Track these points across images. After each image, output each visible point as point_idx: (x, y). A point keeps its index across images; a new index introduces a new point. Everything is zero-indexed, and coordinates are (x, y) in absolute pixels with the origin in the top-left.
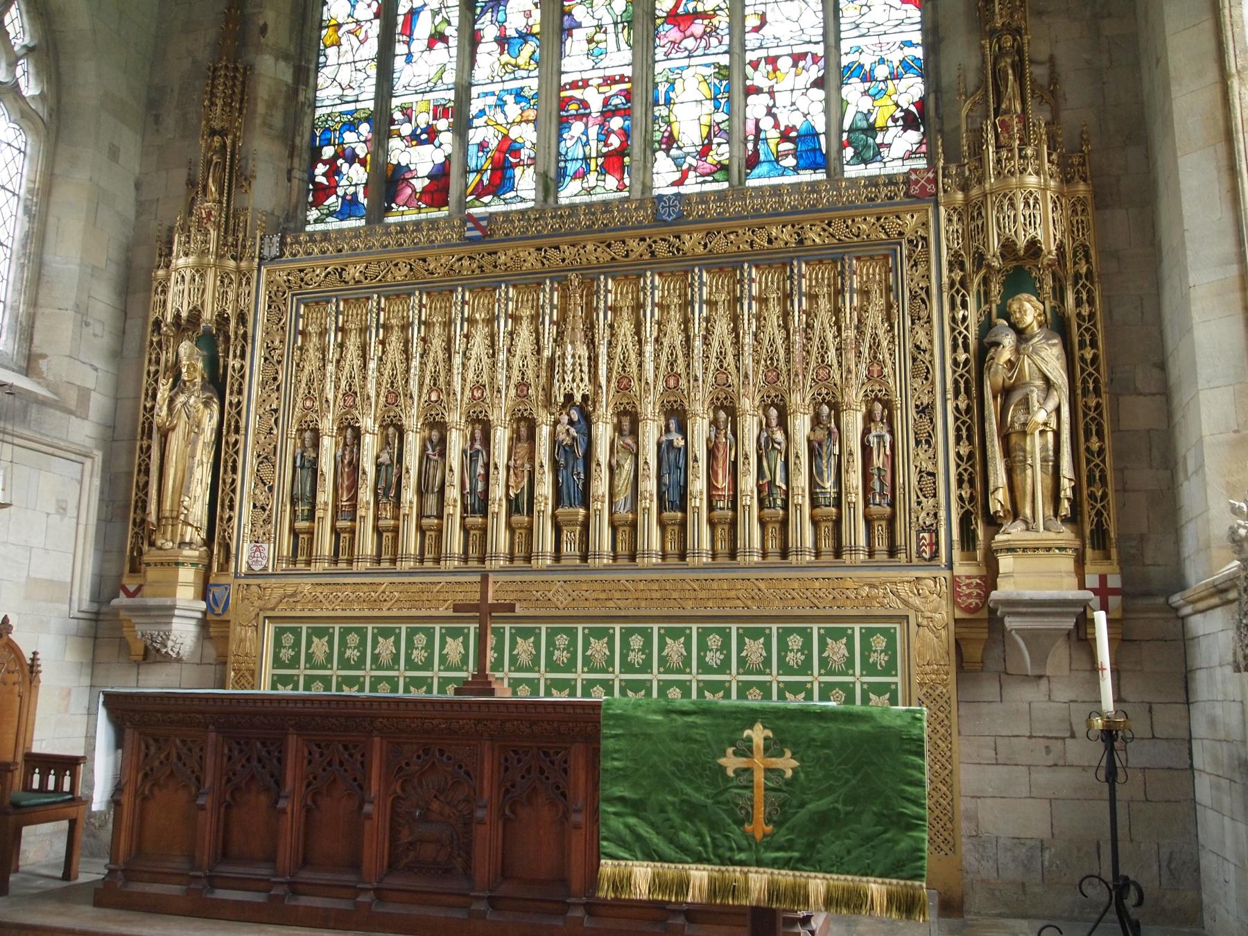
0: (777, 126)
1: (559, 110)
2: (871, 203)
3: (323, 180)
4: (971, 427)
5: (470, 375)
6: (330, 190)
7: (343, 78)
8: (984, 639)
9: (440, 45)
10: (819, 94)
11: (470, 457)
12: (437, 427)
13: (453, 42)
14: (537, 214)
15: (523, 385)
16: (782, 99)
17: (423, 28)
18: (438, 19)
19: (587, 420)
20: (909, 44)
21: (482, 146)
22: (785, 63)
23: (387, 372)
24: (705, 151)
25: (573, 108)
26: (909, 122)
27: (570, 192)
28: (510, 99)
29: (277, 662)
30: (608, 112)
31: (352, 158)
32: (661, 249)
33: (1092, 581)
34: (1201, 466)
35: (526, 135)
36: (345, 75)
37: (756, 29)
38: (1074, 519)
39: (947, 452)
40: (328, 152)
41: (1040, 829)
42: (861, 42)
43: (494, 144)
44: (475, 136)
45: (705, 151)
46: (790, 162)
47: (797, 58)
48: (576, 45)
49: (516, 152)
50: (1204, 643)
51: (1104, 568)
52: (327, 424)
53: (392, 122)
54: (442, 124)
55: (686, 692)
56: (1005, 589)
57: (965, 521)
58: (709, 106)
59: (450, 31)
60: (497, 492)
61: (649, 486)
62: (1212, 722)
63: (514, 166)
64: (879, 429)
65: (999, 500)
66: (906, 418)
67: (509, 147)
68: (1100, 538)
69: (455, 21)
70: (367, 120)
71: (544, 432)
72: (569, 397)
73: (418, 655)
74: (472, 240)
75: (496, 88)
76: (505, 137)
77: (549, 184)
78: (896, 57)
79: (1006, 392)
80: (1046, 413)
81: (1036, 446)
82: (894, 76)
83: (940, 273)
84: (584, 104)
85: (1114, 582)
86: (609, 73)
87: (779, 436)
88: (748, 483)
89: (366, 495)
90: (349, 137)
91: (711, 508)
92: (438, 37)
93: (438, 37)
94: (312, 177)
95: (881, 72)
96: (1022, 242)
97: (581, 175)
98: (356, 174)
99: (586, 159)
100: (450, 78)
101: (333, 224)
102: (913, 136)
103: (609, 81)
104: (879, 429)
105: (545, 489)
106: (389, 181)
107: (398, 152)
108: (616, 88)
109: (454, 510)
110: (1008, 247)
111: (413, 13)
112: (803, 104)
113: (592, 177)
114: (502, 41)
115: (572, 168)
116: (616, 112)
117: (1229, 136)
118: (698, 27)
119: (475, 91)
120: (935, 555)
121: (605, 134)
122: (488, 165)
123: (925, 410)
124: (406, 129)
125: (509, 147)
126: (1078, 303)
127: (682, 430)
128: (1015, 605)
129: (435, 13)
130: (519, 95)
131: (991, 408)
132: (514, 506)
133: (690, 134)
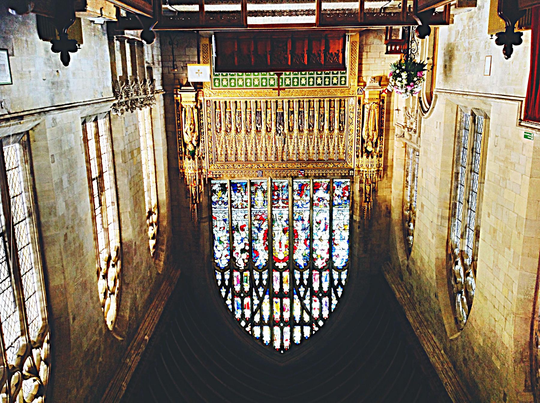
0: (241, 193)
3: (346, 191)
4: (200, 126)
5: (303, 141)
6: (344, 189)
7: (342, 217)
9: (318, 221)
10: (233, 199)
12: (311, 131)
13: (314, 222)
16: (240, 199)
17: (322, 226)
18: (319, 228)
20: (215, 208)
21: (306, 196)
23: (323, 143)
24: (257, 189)
25: (285, 202)
26: (215, 191)
28: (300, 206)
29: (345, 77)
30: (278, 200)
33: (179, 96)
34: (161, 115)
35: (296, 197)
36: (342, 217)
37: (246, 215)
38: (182, 107)
39: (205, 120)
40: (345, 198)
42: (224, 210)
43: (304, 196)
44: (308, 198)
45: (257, 189)
46: (238, 185)
47: (237, 208)
48: (285, 217)
49: (298, 193)
50: (160, 84)
51: (177, 98)
52: (336, 131)
53: (329, 204)
54: (316, 202)
55: (222, 74)
56: (194, 94)
57: (201, 107)
58: (255, 199)
59: (315, 224)
60: (296, 116)
61: (263, 116)
62: (158, 70)
63: (299, 190)
65: (195, 111)
66: (213, 129)
68: (178, 104)
69: (314, 226)
70: (335, 205)
71: (286, 128)
72: (280, 135)
74: (302, 170)
75: (303, 209)
76: (301, 197)
78: (217, 206)
79: (194, 132)
80: (187, 127)
81: (189, 122)
82: (218, 201)
83: (207, 156)
84: (283, 203)
85: (175, 96)
86: (278, 209)
87: (237, 126)
88: (243, 117)
89: (327, 115)
90: (340, 202)
91: (251, 112)
92: (319, 223)
93: (319, 223)
94: (349, 192)
95: (220, 203)
96: (191, 159)
98: (338, 192)
99: (282, 190)
100: (315, 213)
101: (343, 181)
102: (214, 188)
103: (278, 207)
105: (286, 116)
106: (329, 189)
107: (327, 196)
108: (276, 205)
112: (236, 198)
113: (281, 186)
114: (303, 220)
115: (285, 188)
116: (276, 200)
117: (155, 165)
118: (258, 217)
119: (309, 209)
120: (207, 101)
121: (278, 195)
122: (305, 191)
124: (325, 202)
125: (300, 195)
126: (182, 148)
127: (257, 128)
129: (319, 229)
130: (298, 207)
131: (197, 129)
132: (293, 112)
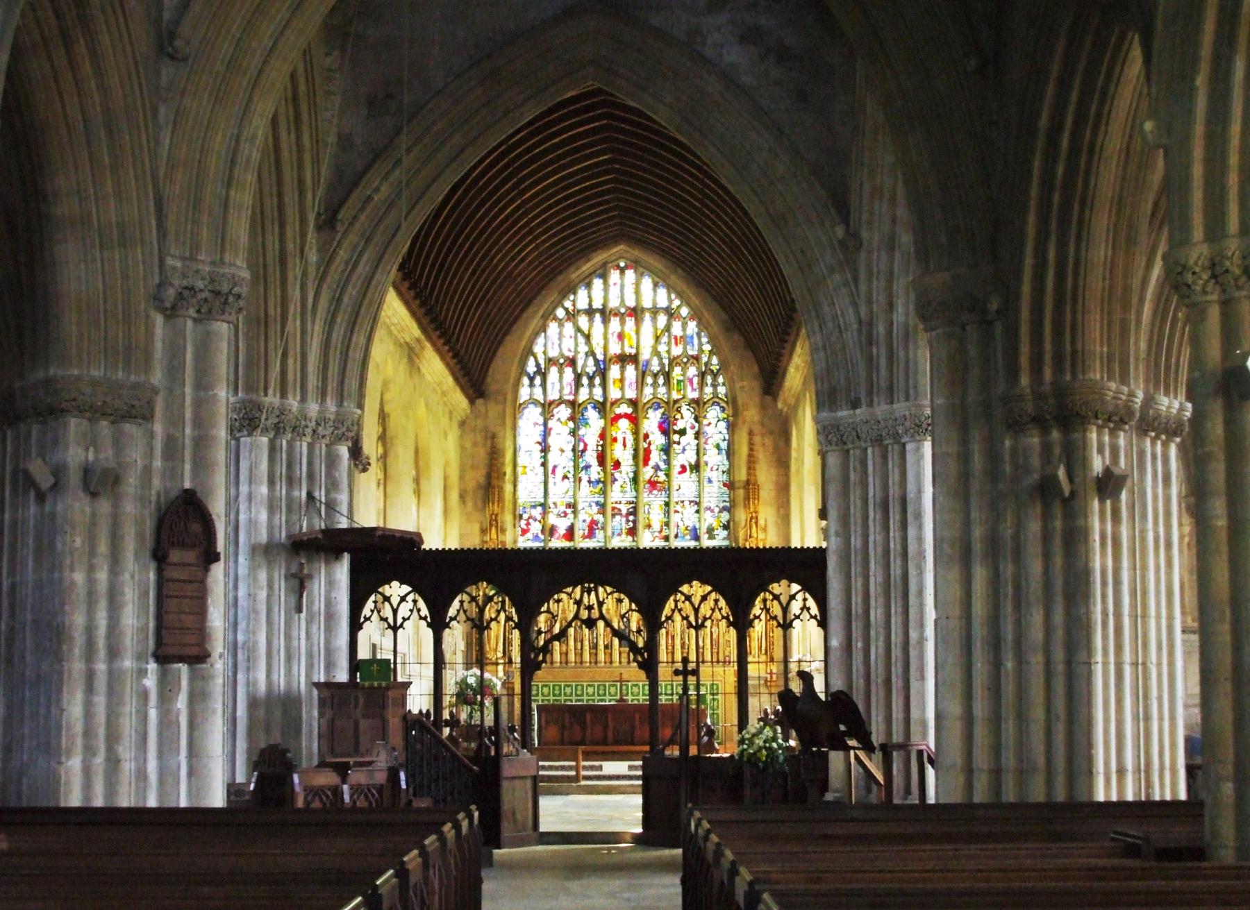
2: (641, 436)
17: (560, 473)
22: (687, 503)
24: (661, 531)
59: (570, 475)
73: (669, 692)
92: (565, 477)
93: (565, 477)
100: (571, 493)
102: (726, 532)
107: (552, 519)
109: (587, 648)
121: (628, 521)
124: (556, 511)
132: (606, 647)
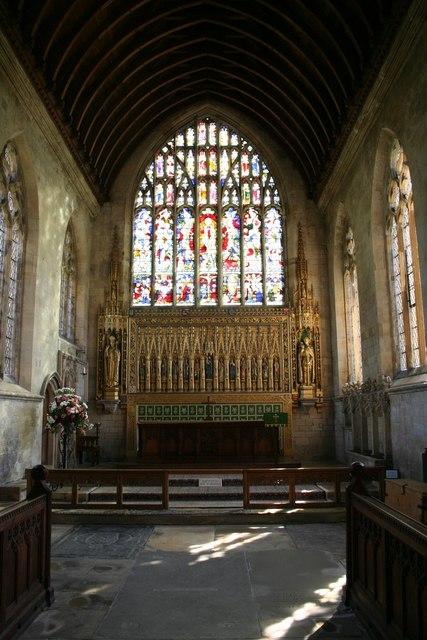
1: (197, 281)
8: (299, 404)
11: (185, 366)
14: (190, 308)
15: (197, 351)
17: (163, 254)
19: (213, 359)
22: (254, 276)
27: (203, 303)
30: (212, 283)
31: (145, 287)
32: (230, 322)
36: (142, 265)
39: (291, 369)
40: (138, 285)
41: (308, 443)
44: (178, 285)
47: (257, 275)
48: (203, 264)
59: (171, 257)
64: (276, 363)
67: (187, 289)
77: (197, 300)
92: (167, 258)
93: (167, 258)
95: (275, 280)
97: (205, 298)
101: (140, 304)
104: (276, 363)
107: (157, 287)
110: (303, 327)
111: (160, 250)
114: (184, 261)
121: (211, 288)
123: (286, 360)
124: (160, 281)
125: (187, 289)
128: (305, 400)
131: (300, 360)
132: (196, 378)
133: (232, 291)
